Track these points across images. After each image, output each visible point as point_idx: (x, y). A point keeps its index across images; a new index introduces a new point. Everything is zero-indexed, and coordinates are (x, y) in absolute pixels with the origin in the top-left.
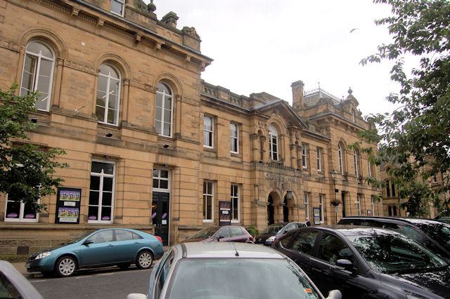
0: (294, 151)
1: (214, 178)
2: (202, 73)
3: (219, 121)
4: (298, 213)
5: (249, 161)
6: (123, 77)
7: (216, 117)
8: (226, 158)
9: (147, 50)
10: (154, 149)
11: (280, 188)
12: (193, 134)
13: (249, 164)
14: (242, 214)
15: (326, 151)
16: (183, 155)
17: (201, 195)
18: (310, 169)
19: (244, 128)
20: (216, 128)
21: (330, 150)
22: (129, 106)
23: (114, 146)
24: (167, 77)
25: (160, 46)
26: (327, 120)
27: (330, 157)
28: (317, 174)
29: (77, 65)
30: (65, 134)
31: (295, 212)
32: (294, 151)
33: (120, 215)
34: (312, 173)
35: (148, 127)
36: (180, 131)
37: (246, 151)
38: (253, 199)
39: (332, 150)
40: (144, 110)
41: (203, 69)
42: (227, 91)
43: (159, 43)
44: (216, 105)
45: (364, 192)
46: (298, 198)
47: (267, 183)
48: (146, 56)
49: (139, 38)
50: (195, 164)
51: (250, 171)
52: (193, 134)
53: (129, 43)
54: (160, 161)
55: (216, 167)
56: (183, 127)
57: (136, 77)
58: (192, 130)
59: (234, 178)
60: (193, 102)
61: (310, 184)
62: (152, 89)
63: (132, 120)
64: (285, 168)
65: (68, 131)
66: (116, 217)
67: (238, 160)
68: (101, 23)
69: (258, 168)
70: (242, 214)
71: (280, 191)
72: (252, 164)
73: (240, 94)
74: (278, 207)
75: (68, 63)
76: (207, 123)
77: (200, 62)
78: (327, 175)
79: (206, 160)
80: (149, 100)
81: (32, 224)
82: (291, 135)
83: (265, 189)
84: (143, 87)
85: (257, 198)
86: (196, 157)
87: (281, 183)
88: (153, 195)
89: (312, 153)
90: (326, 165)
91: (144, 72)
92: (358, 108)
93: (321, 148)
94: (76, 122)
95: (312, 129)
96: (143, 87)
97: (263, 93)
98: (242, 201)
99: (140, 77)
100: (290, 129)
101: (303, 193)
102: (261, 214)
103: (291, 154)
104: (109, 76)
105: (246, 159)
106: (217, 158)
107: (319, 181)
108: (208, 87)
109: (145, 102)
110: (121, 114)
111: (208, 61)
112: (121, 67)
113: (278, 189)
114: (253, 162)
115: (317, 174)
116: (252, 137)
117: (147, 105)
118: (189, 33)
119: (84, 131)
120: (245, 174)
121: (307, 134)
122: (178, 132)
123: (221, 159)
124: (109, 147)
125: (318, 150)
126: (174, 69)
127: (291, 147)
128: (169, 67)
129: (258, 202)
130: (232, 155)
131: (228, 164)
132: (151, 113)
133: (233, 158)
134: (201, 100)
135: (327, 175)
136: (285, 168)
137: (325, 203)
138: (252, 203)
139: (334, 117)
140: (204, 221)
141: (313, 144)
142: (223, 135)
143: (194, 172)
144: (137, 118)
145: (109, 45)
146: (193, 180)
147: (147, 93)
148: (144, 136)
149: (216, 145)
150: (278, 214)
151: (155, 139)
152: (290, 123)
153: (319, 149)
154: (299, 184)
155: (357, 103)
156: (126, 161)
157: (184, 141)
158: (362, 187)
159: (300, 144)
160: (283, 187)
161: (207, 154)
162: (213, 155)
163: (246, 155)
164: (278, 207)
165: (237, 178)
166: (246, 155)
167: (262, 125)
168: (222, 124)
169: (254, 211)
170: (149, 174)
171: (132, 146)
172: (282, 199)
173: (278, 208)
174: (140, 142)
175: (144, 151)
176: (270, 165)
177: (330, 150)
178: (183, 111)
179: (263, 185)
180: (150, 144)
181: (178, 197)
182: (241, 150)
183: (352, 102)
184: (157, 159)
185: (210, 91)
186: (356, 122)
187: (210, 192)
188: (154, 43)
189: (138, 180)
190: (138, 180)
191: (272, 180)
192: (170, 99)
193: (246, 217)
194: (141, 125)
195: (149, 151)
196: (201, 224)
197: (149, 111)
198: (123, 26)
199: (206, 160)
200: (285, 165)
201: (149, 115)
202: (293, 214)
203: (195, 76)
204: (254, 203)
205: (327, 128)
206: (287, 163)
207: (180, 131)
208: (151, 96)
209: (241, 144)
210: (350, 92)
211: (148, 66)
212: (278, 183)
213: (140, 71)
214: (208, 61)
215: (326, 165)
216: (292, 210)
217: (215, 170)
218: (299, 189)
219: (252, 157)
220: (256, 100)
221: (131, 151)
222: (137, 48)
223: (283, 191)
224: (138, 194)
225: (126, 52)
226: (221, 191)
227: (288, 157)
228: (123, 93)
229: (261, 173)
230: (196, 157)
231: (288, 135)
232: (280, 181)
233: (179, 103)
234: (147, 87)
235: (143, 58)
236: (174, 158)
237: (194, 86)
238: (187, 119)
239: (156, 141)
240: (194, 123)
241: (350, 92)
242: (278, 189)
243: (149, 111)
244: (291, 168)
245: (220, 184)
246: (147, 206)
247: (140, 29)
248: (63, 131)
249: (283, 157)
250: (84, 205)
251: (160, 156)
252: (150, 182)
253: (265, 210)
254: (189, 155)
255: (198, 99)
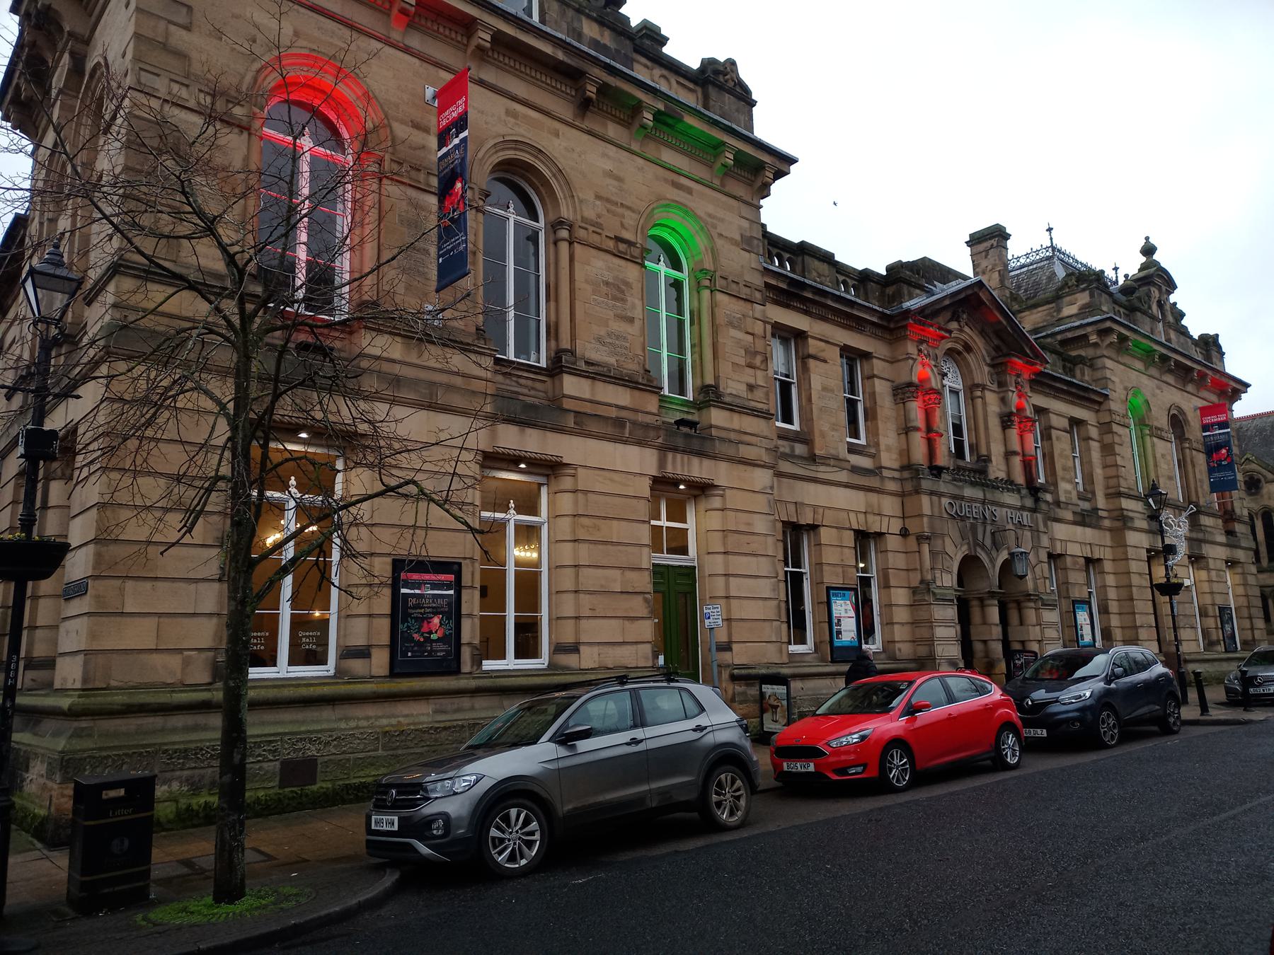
0: (1014, 433)
1: (807, 519)
2: (762, 202)
3: (813, 346)
4: (1038, 617)
5: (896, 465)
6: (552, 217)
7: (800, 336)
8: (837, 459)
9: (612, 130)
10: (652, 434)
11: (988, 542)
12: (751, 387)
13: (897, 475)
14: (888, 623)
15: (1094, 432)
16: (731, 451)
17: (781, 569)
18: (1056, 484)
19: (878, 366)
20: (804, 369)
21: (1106, 428)
22: (578, 305)
23: (544, 428)
24: (510, 154)
25: (1095, 337)
26: (1094, 338)
27: (1108, 449)
28: (1075, 499)
29: (422, 177)
30: (406, 394)
31: (1031, 615)
32: (1014, 433)
33: (569, 638)
34: (1062, 499)
35: (631, 367)
36: (717, 378)
37: (889, 438)
38: (915, 580)
39: (1115, 428)
40: (617, 316)
41: (764, 191)
42: (827, 258)
43: (649, 108)
44: (805, 300)
45: (1208, 550)
46: (1037, 577)
47: (952, 529)
48: (612, 150)
49: (591, 90)
50: (762, 478)
51: (902, 495)
52: (751, 387)
53: (563, 109)
54: (669, 469)
55: (820, 487)
56: (725, 368)
57: (590, 213)
58: (748, 376)
59: (861, 517)
60: (745, 292)
61: (1060, 531)
62: (636, 252)
63: (590, 350)
64: (994, 485)
65: (414, 383)
66: (347, 653)
67: (865, 462)
68: (484, 37)
69: (926, 484)
70: (888, 623)
71: (989, 554)
72: (906, 474)
73: (860, 266)
74: (981, 600)
75: (723, 282)
76: (779, 359)
77: (759, 167)
78: (1101, 502)
79: (785, 467)
80: (627, 284)
81: (321, 682)
82: (1001, 384)
83: (950, 548)
84: (610, 245)
85: (929, 577)
86: (766, 458)
87: (989, 528)
88: (655, 573)
89: (1058, 438)
90: (1098, 472)
91: (608, 200)
92: (1172, 298)
93: (866, 356)
94: (433, 356)
95: (1052, 366)
96: (610, 245)
97: (924, 260)
98: (885, 585)
99: (599, 216)
100: (999, 367)
101: (1044, 557)
102: (945, 623)
103: (1005, 441)
104: (306, 142)
105: (889, 459)
106: (812, 458)
107: (1086, 519)
108: (776, 245)
109: (618, 290)
110: (553, 331)
111: (781, 164)
112: (546, 183)
113: (983, 547)
114: (908, 466)
115: (1075, 499)
116: (902, 392)
117: (624, 300)
118: (721, 78)
119: (458, 381)
120: (890, 505)
121: (1042, 383)
122: (710, 380)
123: (825, 460)
124: (529, 431)
125: (1071, 426)
126: (689, 191)
127: (1006, 422)
128: (676, 185)
129: (932, 586)
130: (853, 449)
131: (843, 476)
132: (638, 323)
133: (856, 460)
134: (767, 285)
135: (1101, 502)
136: (994, 485)
137: (1103, 588)
138: (914, 591)
139: (597, 72)
140: (794, 648)
141: (1061, 410)
142: (825, 389)
143: (760, 503)
144: (599, 340)
145: (509, 113)
146: (761, 525)
147: (622, 262)
148: (620, 396)
149: (807, 419)
150: (985, 623)
151: (652, 404)
152: (997, 349)
153: (1075, 423)
154: (1035, 531)
155: (1171, 285)
156: (728, 492)
157: (732, 408)
158: (1200, 536)
159: (1029, 412)
160: (994, 543)
161: (784, 447)
162: (800, 449)
163: (888, 449)
164: (981, 600)
165: (1096, 549)
166: (888, 449)
167: (928, 355)
168: (821, 355)
169: (923, 614)
170: (643, 509)
171: (593, 427)
172: (994, 573)
173: (983, 606)
174: (613, 413)
175: (625, 442)
176: (959, 473)
177: (1106, 428)
178: (721, 319)
179: (943, 535)
180: (641, 418)
181: (570, 572)
182: (873, 433)
183: (1158, 281)
184: (662, 463)
185: (844, 283)
186: (1169, 340)
187: (797, 563)
188: (637, 108)
189: (618, 531)
190: (618, 531)
191: (969, 527)
192: (534, 238)
193: (900, 633)
194: (612, 361)
195: (640, 443)
196: (785, 659)
197: (631, 320)
198: (547, 48)
199: (785, 467)
200: (992, 477)
201: (633, 330)
202: (1022, 623)
203: (746, 211)
204: (922, 592)
205: (1091, 363)
206: (997, 470)
207: (717, 378)
208: (632, 272)
209: (871, 415)
210: (1148, 250)
211: (619, 179)
212: (980, 530)
213: (598, 197)
214: (781, 164)
215: (1098, 472)
216: (1020, 610)
217: (813, 495)
218: (1036, 547)
219: (906, 452)
220: (909, 283)
221: (592, 443)
222: (587, 124)
223: (994, 553)
224: (616, 574)
225: (557, 135)
226: (830, 556)
227: (997, 450)
228: (554, 265)
229: (935, 498)
230: (766, 458)
231: (995, 387)
232: (984, 523)
233: (564, 247)
234: (622, 247)
235: (604, 155)
236: (707, 463)
237: (746, 243)
238: (733, 339)
239: (654, 409)
240: (752, 353)
241: (1148, 250)
242: (983, 547)
243: (631, 320)
244: (1009, 484)
245: (826, 535)
246: (644, 612)
247: (596, 61)
248: (397, 381)
249: (984, 451)
250: (470, 615)
251: (670, 455)
252: (645, 535)
253: (951, 612)
254: (745, 452)
255: (758, 280)
